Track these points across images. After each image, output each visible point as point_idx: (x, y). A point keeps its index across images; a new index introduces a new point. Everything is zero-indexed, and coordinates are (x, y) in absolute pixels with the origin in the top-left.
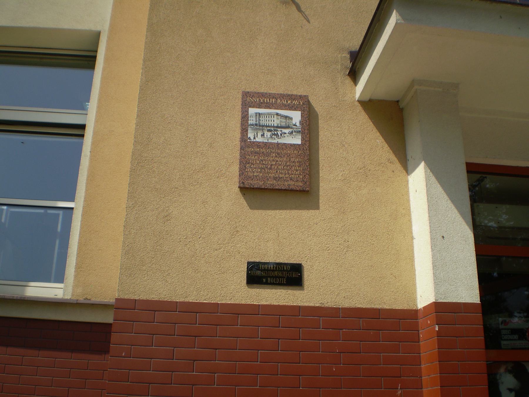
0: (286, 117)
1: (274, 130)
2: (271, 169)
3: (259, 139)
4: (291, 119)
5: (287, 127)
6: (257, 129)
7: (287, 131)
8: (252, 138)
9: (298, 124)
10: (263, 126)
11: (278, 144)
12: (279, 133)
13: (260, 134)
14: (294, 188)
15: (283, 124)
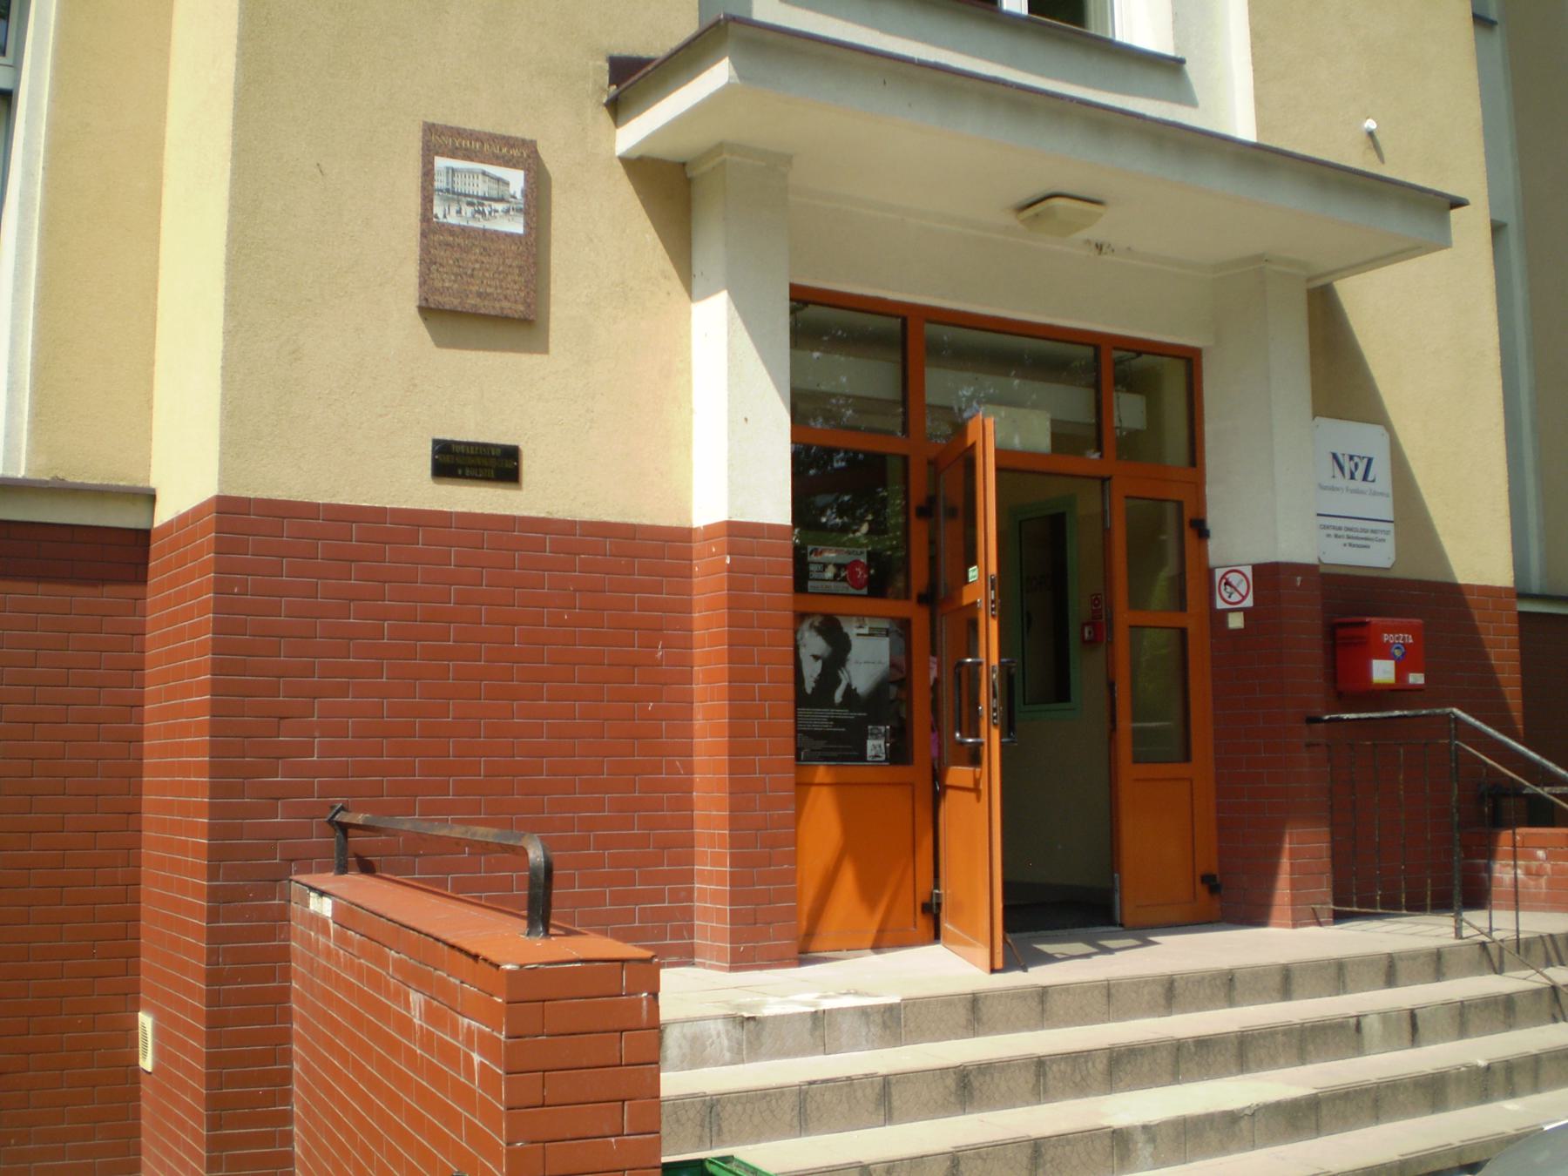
0: (499, 180)
1: (478, 203)
2: (472, 276)
3: (453, 219)
4: (507, 184)
5: (501, 200)
6: (448, 199)
7: (500, 207)
8: (440, 215)
9: (519, 195)
10: (459, 194)
11: (485, 231)
12: (487, 210)
13: (454, 210)
14: (507, 312)
15: (494, 194)
